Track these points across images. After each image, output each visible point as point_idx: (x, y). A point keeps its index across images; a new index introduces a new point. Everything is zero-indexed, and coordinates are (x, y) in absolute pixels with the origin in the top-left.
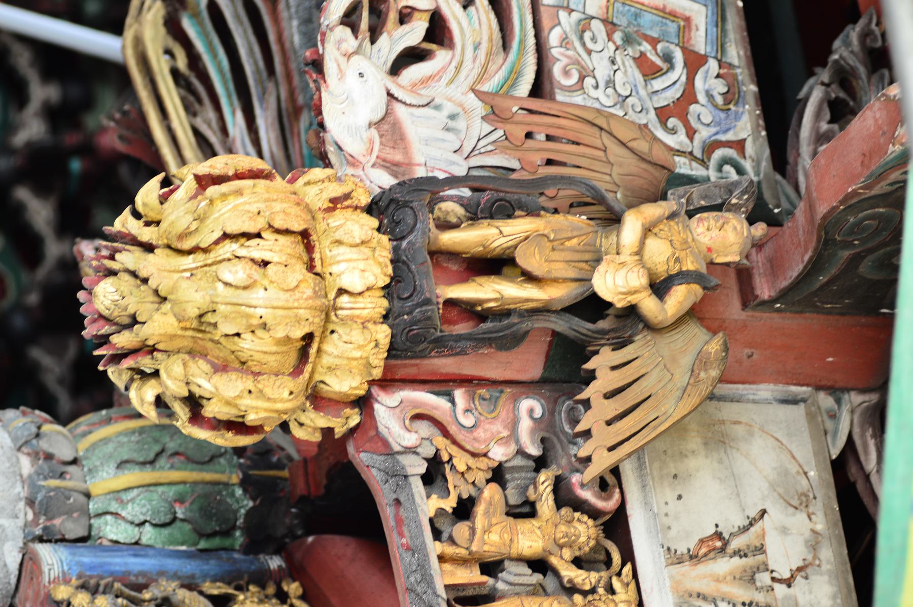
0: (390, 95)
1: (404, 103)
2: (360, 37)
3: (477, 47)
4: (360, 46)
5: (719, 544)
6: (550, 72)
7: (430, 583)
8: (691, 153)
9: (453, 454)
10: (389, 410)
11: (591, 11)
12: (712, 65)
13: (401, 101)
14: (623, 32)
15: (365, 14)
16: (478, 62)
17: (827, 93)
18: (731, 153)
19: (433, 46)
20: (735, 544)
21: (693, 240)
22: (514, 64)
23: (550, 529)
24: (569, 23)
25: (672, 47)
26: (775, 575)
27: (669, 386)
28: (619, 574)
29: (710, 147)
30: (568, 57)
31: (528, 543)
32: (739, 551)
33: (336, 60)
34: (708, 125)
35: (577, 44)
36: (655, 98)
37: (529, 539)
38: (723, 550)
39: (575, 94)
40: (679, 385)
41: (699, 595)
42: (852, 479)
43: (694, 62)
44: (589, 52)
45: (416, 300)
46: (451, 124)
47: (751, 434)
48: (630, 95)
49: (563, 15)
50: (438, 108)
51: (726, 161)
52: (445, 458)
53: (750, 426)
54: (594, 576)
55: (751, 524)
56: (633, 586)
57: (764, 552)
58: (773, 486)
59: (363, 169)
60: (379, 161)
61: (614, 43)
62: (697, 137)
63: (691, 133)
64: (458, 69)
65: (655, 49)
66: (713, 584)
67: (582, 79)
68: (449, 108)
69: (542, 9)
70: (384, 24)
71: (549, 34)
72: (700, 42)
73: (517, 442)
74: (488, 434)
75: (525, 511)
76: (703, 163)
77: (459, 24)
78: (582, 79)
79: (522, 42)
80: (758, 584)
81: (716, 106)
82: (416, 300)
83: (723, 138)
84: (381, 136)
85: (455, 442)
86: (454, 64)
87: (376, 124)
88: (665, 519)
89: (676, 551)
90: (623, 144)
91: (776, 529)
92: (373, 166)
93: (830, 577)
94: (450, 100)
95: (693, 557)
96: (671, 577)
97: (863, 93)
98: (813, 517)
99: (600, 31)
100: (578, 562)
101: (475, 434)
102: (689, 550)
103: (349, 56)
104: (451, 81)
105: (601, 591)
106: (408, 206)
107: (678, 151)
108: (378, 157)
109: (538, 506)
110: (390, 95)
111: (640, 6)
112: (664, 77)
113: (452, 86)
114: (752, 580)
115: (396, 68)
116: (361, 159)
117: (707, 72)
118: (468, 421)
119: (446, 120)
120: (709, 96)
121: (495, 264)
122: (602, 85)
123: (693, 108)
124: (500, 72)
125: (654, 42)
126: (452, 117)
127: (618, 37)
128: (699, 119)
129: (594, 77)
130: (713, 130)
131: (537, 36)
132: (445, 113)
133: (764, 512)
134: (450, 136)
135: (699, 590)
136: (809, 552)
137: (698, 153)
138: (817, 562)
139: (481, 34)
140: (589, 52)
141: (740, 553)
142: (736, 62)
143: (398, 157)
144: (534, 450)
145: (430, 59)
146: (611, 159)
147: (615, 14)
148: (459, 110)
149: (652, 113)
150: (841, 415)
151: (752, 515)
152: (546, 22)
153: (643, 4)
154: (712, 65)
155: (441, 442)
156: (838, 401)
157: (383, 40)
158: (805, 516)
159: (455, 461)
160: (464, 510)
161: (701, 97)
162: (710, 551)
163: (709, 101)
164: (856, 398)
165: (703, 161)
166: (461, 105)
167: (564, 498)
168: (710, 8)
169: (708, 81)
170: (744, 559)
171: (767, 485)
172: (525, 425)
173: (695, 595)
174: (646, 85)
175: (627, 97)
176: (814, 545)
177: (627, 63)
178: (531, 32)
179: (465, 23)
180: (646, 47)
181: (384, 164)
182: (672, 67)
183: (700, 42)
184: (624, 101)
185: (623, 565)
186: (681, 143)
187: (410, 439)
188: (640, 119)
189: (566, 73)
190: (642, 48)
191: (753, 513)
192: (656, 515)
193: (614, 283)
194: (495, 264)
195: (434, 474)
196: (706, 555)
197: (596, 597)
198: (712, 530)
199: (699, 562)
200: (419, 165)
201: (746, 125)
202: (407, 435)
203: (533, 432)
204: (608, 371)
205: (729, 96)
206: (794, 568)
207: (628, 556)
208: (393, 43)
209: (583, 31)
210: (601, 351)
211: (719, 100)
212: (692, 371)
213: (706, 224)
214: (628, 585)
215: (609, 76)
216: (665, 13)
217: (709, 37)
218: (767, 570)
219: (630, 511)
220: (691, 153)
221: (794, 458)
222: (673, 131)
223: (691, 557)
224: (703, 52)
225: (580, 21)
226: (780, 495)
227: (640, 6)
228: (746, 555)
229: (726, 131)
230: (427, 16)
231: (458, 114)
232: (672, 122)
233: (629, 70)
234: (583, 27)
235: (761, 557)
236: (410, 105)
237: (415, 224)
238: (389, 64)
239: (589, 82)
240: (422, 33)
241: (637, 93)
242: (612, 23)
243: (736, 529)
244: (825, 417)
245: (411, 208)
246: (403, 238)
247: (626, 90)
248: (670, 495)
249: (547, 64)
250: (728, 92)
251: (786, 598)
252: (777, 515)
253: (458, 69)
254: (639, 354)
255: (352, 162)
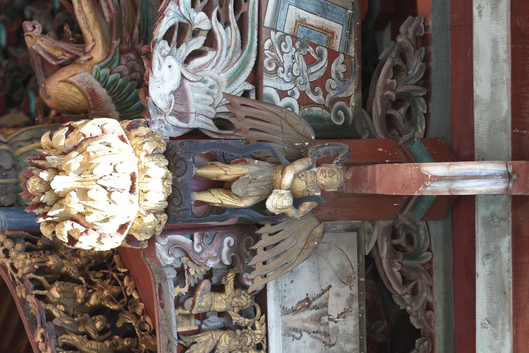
0: (182, 75)
1: (189, 80)
2: (172, 45)
3: (229, 48)
4: (171, 50)
5: (307, 304)
6: (263, 62)
7: (170, 330)
8: (324, 105)
9: (190, 266)
10: (160, 246)
11: (286, 31)
12: (342, 57)
13: (188, 79)
14: (301, 42)
15: (176, 33)
16: (228, 57)
17: (393, 62)
18: (343, 103)
19: (207, 48)
20: (314, 304)
21: (317, 181)
22: (245, 57)
23: (230, 300)
24: (275, 38)
25: (323, 48)
26: (330, 317)
27: (295, 247)
28: (259, 320)
29: (333, 101)
30: (272, 56)
31: (219, 307)
32: (316, 306)
33: (159, 59)
34: (334, 90)
35: (277, 49)
36: (311, 76)
37: (220, 302)
38: (308, 306)
39: (272, 76)
40: (300, 247)
41: (294, 329)
42: (374, 257)
43: (333, 55)
44: (282, 53)
45: (182, 207)
46: (211, 91)
47: (330, 248)
48: (299, 76)
49: (272, 33)
50: (205, 82)
51: (340, 108)
52: (186, 267)
53: (330, 244)
54: (247, 320)
55: (323, 293)
56: (264, 326)
57: (327, 306)
58: (336, 273)
59: (165, 117)
60: (173, 112)
61: (295, 48)
62: (328, 96)
63: (325, 94)
64: (218, 61)
65: (315, 50)
66: (301, 323)
67: (277, 68)
68: (211, 82)
69: (263, 29)
70: (184, 37)
71: (264, 42)
72: (337, 46)
73: (221, 258)
74: (207, 255)
75: (218, 288)
76: (329, 110)
77: (221, 37)
78: (277, 68)
79: (251, 46)
80: (322, 322)
81: (339, 79)
82: (182, 207)
83: (340, 96)
84: (176, 99)
85: (191, 260)
86: (216, 58)
87: (174, 93)
88: (284, 293)
89: (287, 308)
90: (291, 126)
91: (334, 294)
92: (169, 115)
93: (355, 316)
94: (211, 78)
95: (294, 311)
96: (283, 321)
97: (410, 60)
98: (352, 288)
99: (289, 41)
100: (241, 313)
101: (201, 256)
102: (293, 307)
103: (164, 57)
104: (214, 67)
105: (249, 328)
106: (183, 160)
107: (318, 104)
108: (173, 110)
109: (226, 287)
110: (182, 75)
111: (310, 27)
112: (317, 65)
113: (214, 70)
114: (320, 320)
115: (187, 61)
116: (165, 111)
117: (338, 61)
118: (198, 250)
119: (208, 89)
120: (337, 74)
121: (223, 185)
122: (286, 70)
123: (329, 81)
124: (238, 63)
125: (314, 46)
126: (212, 87)
127: (297, 44)
128: (331, 87)
129: (283, 67)
130: (336, 92)
131: (258, 42)
132: (208, 85)
133: (330, 286)
134: (209, 97)
135: (294, 327)
136: (348, 305)
137: (327, 105)
138: (351, 310)
139: (231, 42)
140: (282, 53)
141: (316, 308)
142: (353, 55)
143: (183, 110)
144: (227, 263)
145: (205, 56)
146: (284, 131)
147: (298, 32)
148: (215, 83)
149: (308, 84)
150: (373, 232)
151: (324, 288)
152: (264, 36)
153: (312, 26)
154: (342, 57)
155: (185, 259)
156: (373, 225)
157: (183, 47)
158: (348, 287)
159: (190, 270)
160: (193, 291)
161: (333, 75)
162: (302, 307)
163: (337, 77)
164: (383, 224)
165: (329, 109)
166: (216, 80)
167: (239, 285)
168: (345, 26)
169: (338, 67)
170: (317, 310)
171: (333, 273)
172: (226, 249)
173: (292, 329)
174: (308, 70)
175: (297, 77)
176: (350, 302)
177: (300, 59)
178: (256, 40)
179: (224, 37)
180: (310, 49)
181: (176, 113)
182: (322, 60)
183: (337, 46)
184: (296, 79)
185: (261, 315)
186: (319, 100)
187: (170, 260)
188: (302, 88)
189: (270, 64)
190: (309, 50)
191: (324, 287)
192: (280, 291)
193: (277, 202)
194: (223, 185)
195: (181, 272)
196: (300, 309)
197: (247, 331)
198: (304, 297)
199: (296, 313)
200: (192, 113)
201: (352, 89)
202: (169, 259)
203: (229, 253)
204: (268, 236)
205: (347, 73)
206: (339, 313)
207: (264, 311)
208: (188, 47)
209: (281, 42)
210: (265, 225)
211: (342, 76)
212: (307, 242)
213: (324, 175)
214: (262, 325)
215: (290, 66)
216: (322, 30)
217: (342, 42)
218: (327, 315)
219: (268, 288)
220: (324, 105)
221: (348, 259)
222: (316, 94)
223: (293, 311)
224: (338, 51)
225: (281, 36)
226: (338, 277)
227: (310, 27)
228: (318, 309)
229: (342, 93)
230: (206, 33)
231: (214, 85)
232: (317, 89)
233: (301, 62)
234: (282, 39)
235: (325, 309)
236: (192, 81)
237: (186, 171)
238: (184, 59)
239: (281, 69)
240: (202, 42)
241: (303, 74)
242: (296, 37)
243: (316, 296)
244: (366, 234)
245: (185, 161)
246: (179, 176)
247: (297, 73)
248: (287, 281)
249: (261, 58)
250: (346, 72)
251: (334, 328)
252: (335, 288)
253: (218, 61)
254: (283, 228)
255: (159, 112)
